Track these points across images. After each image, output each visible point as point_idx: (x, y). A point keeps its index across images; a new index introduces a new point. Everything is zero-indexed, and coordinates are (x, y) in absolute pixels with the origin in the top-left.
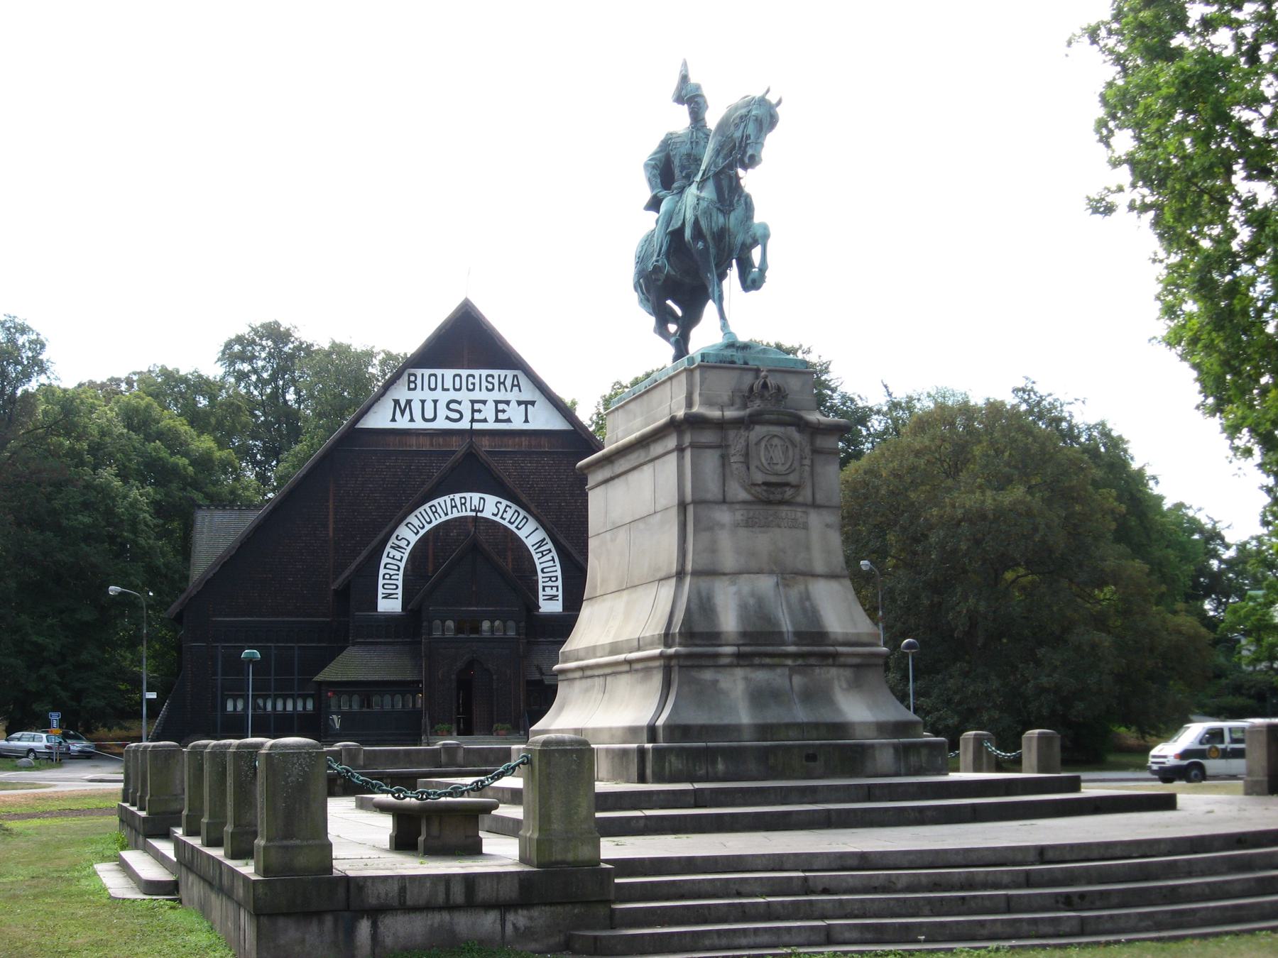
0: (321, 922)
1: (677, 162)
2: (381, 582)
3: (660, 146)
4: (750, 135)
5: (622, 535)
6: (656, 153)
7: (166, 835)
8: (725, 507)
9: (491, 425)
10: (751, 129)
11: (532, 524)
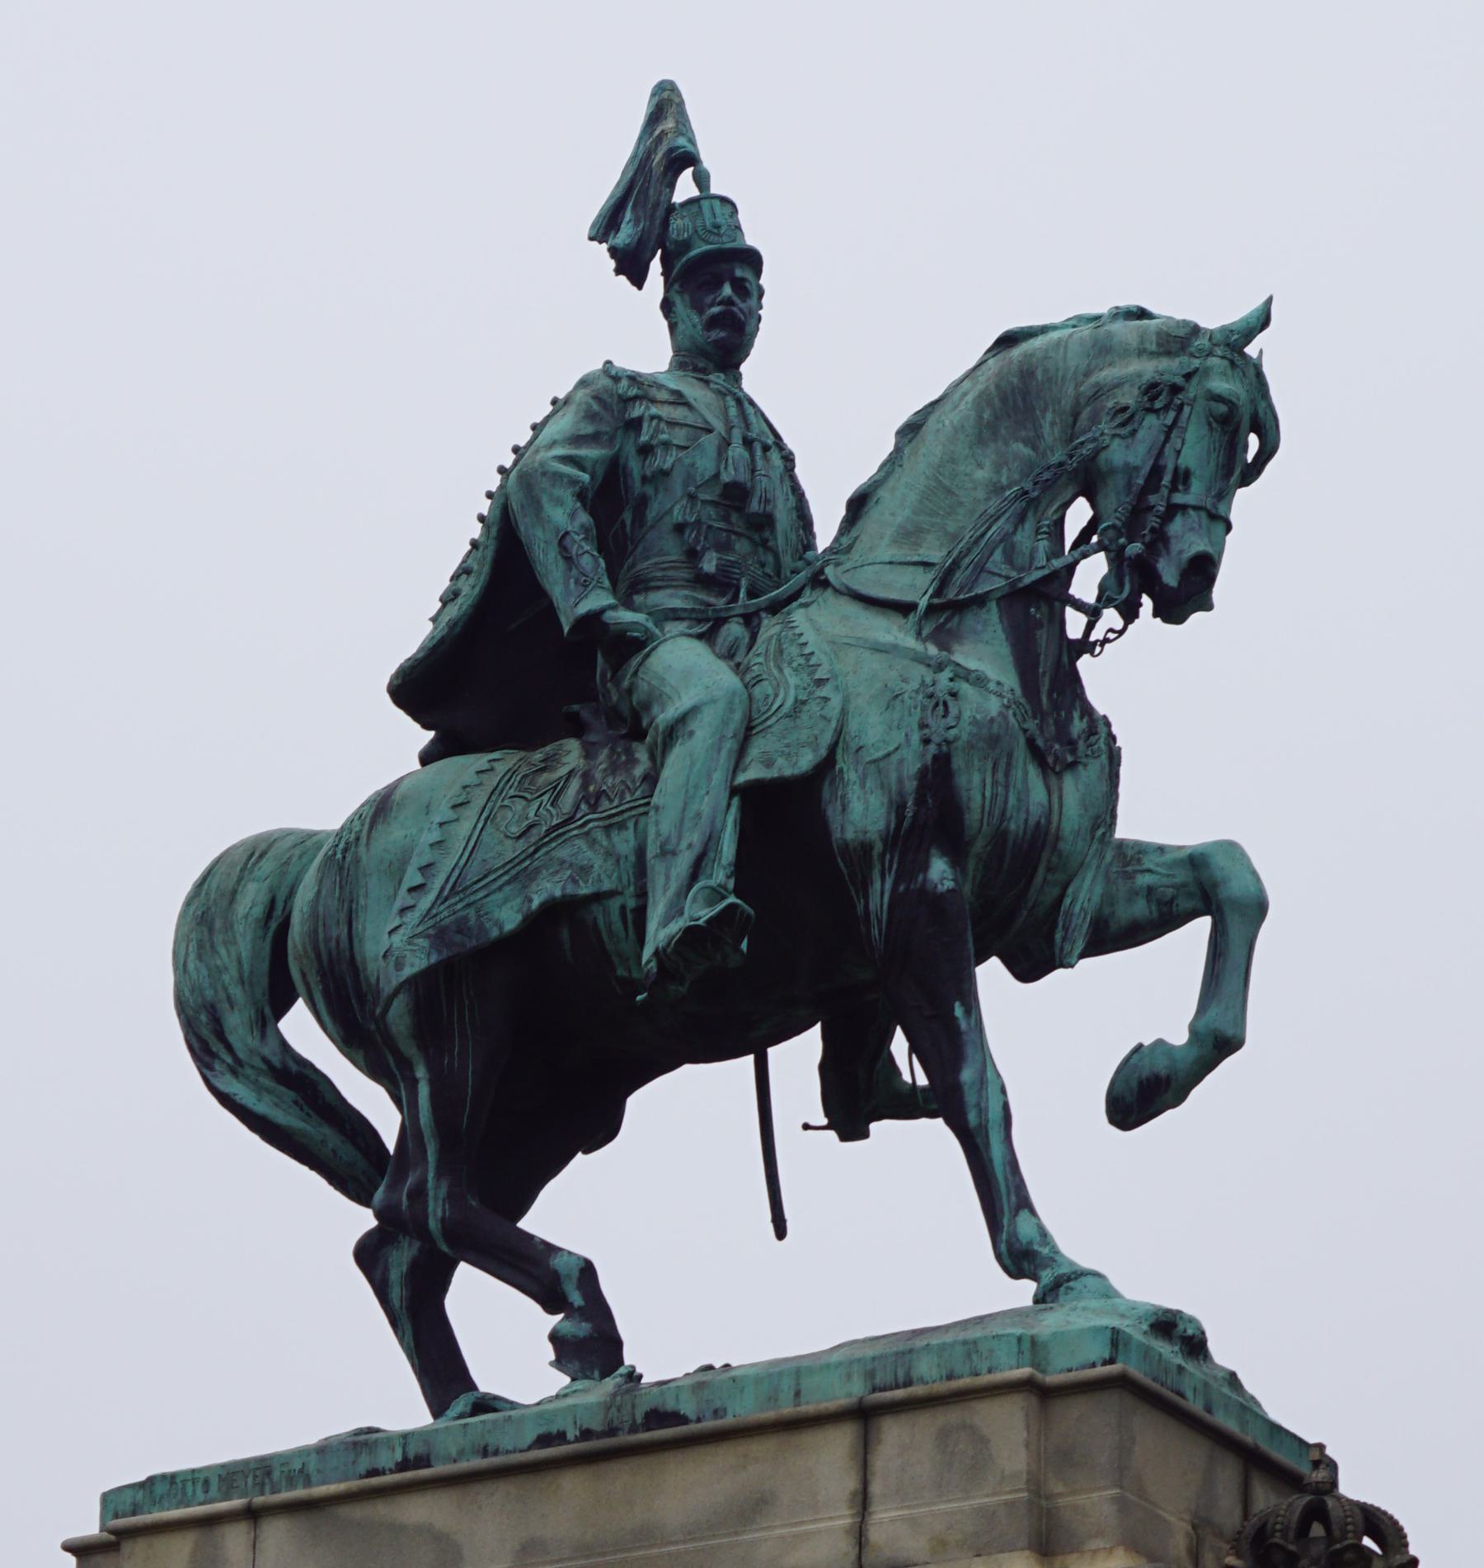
4: (1187, 474)
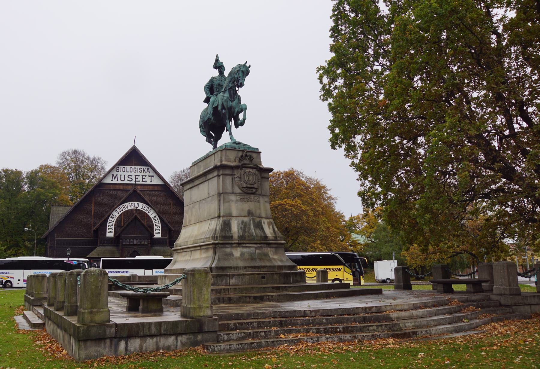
0: (105, 343)
1: (215, 86)
2: (108, 228)
3: (209, 81)
5: (197, 206)
6: (208, 83)
7: (41, 306)
8: (233, 195)
9: (141, 183)
10: (241, 75)
11: (152, 211)
